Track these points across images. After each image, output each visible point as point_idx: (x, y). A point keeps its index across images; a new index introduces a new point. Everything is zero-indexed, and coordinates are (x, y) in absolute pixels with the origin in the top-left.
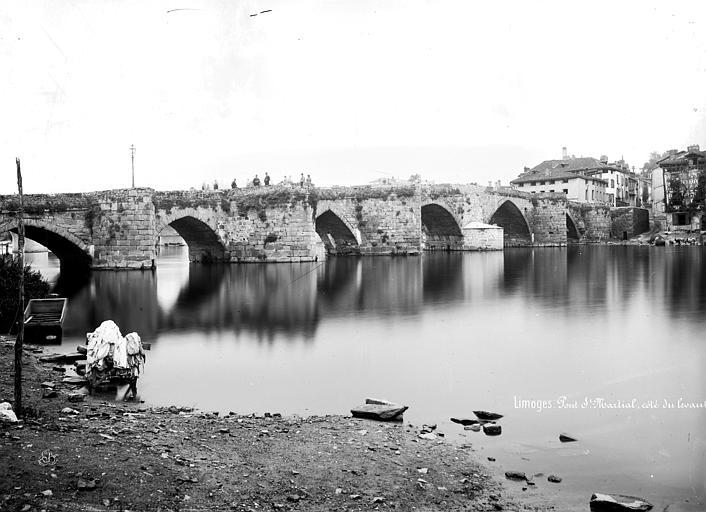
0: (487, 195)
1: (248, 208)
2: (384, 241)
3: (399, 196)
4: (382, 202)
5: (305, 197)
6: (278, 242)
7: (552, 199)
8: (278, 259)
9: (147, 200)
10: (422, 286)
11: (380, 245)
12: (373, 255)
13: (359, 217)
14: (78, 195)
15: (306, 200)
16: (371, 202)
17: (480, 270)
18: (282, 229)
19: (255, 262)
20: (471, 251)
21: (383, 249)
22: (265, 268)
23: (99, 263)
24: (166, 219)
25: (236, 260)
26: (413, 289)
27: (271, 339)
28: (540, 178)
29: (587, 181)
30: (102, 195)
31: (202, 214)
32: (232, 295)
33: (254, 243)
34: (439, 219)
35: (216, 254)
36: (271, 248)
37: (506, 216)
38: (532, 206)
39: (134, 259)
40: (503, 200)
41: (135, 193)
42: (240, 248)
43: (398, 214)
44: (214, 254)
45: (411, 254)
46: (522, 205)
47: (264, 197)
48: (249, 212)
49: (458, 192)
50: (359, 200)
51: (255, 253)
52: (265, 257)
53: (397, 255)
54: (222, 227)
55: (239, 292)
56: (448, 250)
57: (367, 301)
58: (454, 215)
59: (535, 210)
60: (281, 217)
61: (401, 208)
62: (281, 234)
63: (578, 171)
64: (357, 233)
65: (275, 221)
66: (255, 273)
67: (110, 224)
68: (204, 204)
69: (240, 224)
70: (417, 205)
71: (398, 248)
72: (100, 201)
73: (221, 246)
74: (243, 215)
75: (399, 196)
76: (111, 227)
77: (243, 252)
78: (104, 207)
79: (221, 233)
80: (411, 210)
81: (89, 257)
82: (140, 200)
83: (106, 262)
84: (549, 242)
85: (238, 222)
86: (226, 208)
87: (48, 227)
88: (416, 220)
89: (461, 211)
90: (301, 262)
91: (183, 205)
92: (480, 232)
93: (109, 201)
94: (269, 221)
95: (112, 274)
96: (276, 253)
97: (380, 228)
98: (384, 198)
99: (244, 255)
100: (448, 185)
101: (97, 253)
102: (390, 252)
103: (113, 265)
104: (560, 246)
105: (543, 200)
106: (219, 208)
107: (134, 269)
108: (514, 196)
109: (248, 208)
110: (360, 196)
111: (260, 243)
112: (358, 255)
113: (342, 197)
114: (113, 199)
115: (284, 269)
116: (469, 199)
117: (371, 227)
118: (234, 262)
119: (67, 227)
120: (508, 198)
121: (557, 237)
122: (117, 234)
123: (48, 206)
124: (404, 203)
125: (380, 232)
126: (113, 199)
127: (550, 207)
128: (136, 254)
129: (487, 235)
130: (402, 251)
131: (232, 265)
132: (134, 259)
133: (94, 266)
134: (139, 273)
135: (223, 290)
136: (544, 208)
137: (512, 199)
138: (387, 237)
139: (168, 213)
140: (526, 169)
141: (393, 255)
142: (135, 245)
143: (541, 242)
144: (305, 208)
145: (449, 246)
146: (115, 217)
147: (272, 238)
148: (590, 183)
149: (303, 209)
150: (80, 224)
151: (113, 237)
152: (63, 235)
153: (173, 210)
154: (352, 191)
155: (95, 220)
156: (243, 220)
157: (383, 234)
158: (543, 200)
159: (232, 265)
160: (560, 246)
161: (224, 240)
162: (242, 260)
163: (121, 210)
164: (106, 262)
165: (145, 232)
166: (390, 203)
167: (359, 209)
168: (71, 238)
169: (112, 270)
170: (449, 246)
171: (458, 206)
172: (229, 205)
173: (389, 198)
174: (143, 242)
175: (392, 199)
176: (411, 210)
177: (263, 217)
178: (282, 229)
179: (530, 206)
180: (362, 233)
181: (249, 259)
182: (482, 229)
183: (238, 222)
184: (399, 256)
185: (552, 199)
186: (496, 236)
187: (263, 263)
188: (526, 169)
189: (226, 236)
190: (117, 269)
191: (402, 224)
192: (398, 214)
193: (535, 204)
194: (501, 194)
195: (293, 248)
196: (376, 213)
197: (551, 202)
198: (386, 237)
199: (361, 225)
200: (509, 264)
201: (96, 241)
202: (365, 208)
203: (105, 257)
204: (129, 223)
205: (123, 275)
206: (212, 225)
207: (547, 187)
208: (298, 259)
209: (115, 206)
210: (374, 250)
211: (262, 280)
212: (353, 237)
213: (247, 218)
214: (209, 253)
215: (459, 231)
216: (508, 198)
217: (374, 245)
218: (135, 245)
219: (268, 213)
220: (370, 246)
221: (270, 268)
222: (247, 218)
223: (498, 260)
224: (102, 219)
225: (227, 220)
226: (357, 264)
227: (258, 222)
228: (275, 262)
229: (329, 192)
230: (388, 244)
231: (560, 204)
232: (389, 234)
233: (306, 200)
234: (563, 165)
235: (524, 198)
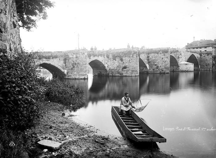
0: (187, 52)
1: (116, 57)
2: (157, 68)
3: (163, 53)
4: (157, 54)
5: (137, 53)
6: (127, 69)
7: (207, 54)
8: (127, 75)
9: (86, 54)
10: (170, 83)
11: (156, 70)
12: (153, 73)
13: (148, 60)
14: (61, 52)
15: (137, 54)
16: (153, 55)
17: (183, 79)
18: (129, 64)
19: (119, 76)
20: (183, 71)
21: (157, 71)
22: (122, 79)
23: (68, 76)
24: (89, 61)
25: (111, 75)
26: (167, 87)
27: (97, 102)
28: (196, 47)
29: (213, 47)
30: (70, 52)
31: (100, 59)
32: (110, 88)
33: (118, 69)
34: (174, 62)
35: (103, 73)
36: (125, 71)
37: (192, 59)
38: (200, 56)
39: (82, 75)
40: (191, 54)
41: (82, 51)
42: (113, 71)
43: (162, 59)
44: (103, 73)
45: (167, 73)
46: (197, 56)
47: (122, 53)
48: (117, 58)
49: (178, 51)
50: (148, 54)
51: (118, 73)
52: (122, 74)
53: (162, 73)
54: (107, 63)
55: (109, 87)
56: (173, 71)
57: (151, 89)
58: (177, 59)
59: (200, 57)
60: (129, 59)
61: (163, 57)
62: (128, 66)
63: (209, 44)
64: (148, 66)
65: (126, 61)
66: (119, 80)
67: (73, 62)
68: (101, 55)
69: (113, 62)
70: (168, 55)
71: (162, 71)
72: (69, 54)
73: (106, 70)
74: (114, 59)
75: (163, 53)
76: (73, 63)
77: (114, 72)
78: (71, 56)
79: (106, 66)
80: (167, 58)
81: (65, 75)
82: (84, 54)
83: (71, 76)
84: (206, 68)
85: (112, 62)
86: (108, 57)
87: (52, 64)
88: (168, 61)
89: (179, 58)
90: (135, 76)
91: (94, 56)
92: (184, 64)
93: (72, 54)
94: (124, 61)
95: (74, 81)
96: (127, 73)
97: (156, 64)
98: (158, 53)
99: (114, 73)
100: (175, 49)
101: (67, 73)
102: (159, 72)
103: (74, 77)
104: (209, 70)
105: (204, 54)
106: (105, 57)
107: (82, 79)
108: (195, 53)
109: (116, 57)
110: (149, 52)
111: (120, 69)
112: (148, 73)
113: (56, 57)
114: (74, 54)
115: (129, 79)
116: (181, 54)
117: (152, 63)
118: (111, 76)
119: (57, 63)
120: (193, 53)
121: (209, 67)
122: (75, 66)
123: (52, 56)
124: (165, 55)
125: (156, 65)
126: (74, 54)
127: (206, 56)
128: (82, 73)
129: (188, 66)
130: (163, 72)
131: (110, 77)
132: (82, 75)
133: (67, 77)
134: (83, 80)
135: (107, 86)
136: (204, 57)
137: (194, 54)
138: (159, 67)
139: (90, 58)
140: (188, 44)
141: (160, 73)
142: (82, 70)
143: (203, 68)
144: (137, 57)
145: (173, 70)
146: (75, 60)
147: (125, 68)
148: (214, 48)
149: (136, 57)
150: (62, 62)
151: (74, 67)
152: (56, 66)
153: (91, 57)
154: (146, 51)
155: (67, 61)
156: (114, 61)
157: (157, 66)
158: (204, 54)
159: (110, 77)
160: (209, 70)
161: (107, 68)
162: (114, 75)
163: (77, 57)
164: (71, 76)
165: (85, 65)
166: (160, 55)
167: (148, 57)
168: (59, 67)
169: (73, 79)
170: (173, 70)
171: (178, 56)
172: (109, 55)
173: (159, 53)
174: (85, 69)
175: (161, 54)
176: (167, 58)
177: (122, 60)
178: (129, 64)
179: (199, 56)
180: (149, 65)
181: (116, 75)
182: (187, 64)
183: (112, 62)
184: (162, 74)
185: (207, 54)
186: (191, 66)
187: (122, 77)
188: (188, 44)
189: (108, 67)
190: (75, 79)
191: (164, 63)
192: (162, 59)
193: (201, 55)
194: (191, 52)
195: (133, 71)
196: (154, 59)
197: (206, 55)
198: (158, 67)
199: (149, 63)
200: (196, 76)
201: (67, 69)
202: (150, 57)
203: (71, 74)
204: (80, 62)
205: (77, 81)
206: (103, 63)
207: (199, 50)
208: (134, 75)
209: (75, 56)
210: (153, 71)
211: (121, 83)
212: (146, 67)
213: (116, 60)
214: (101, 73)
215: (178, 65)
216: (193, 53)
217: (153, 69)
218: (82, 70)
219: (124, 59)
220: (152, 70)
221: (124, 78)
222: (116, 60)
223: (191, 75)
224: (70, 61)
225: (108, 61)
226: (147, 77)
227: (120, 61)
228: (126, 76)
229: (47, 55)
230: (159, 69)
231: (210, 55)
232: (159, 66)
233: (137, 54)
234: (201, 42)
235: (198, 53)
